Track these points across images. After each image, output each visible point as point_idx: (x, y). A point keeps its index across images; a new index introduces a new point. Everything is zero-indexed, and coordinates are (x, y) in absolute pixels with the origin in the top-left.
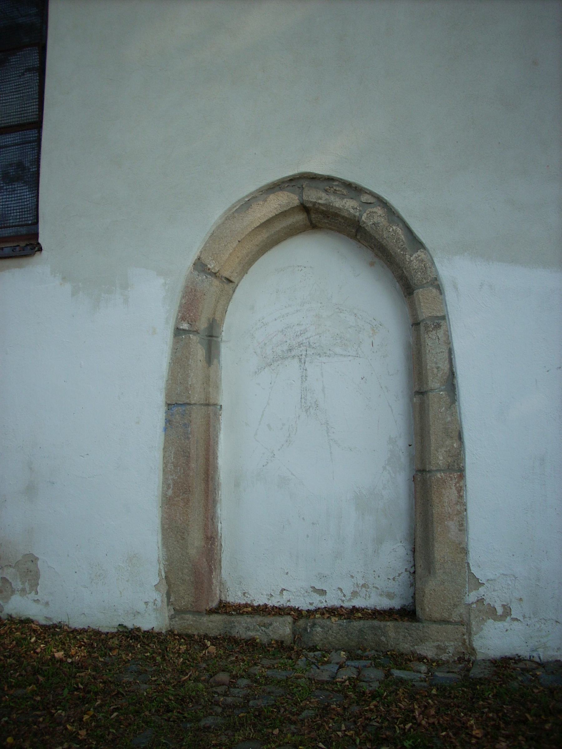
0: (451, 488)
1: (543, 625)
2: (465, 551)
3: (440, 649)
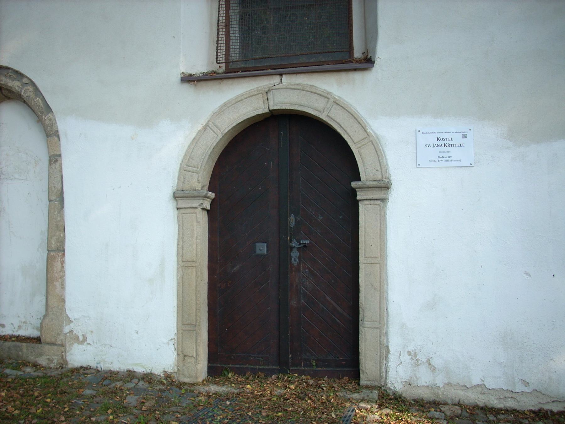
0: (58, 262)
1: (103, 348)
2: (63, 301)
3: (50, 361)
